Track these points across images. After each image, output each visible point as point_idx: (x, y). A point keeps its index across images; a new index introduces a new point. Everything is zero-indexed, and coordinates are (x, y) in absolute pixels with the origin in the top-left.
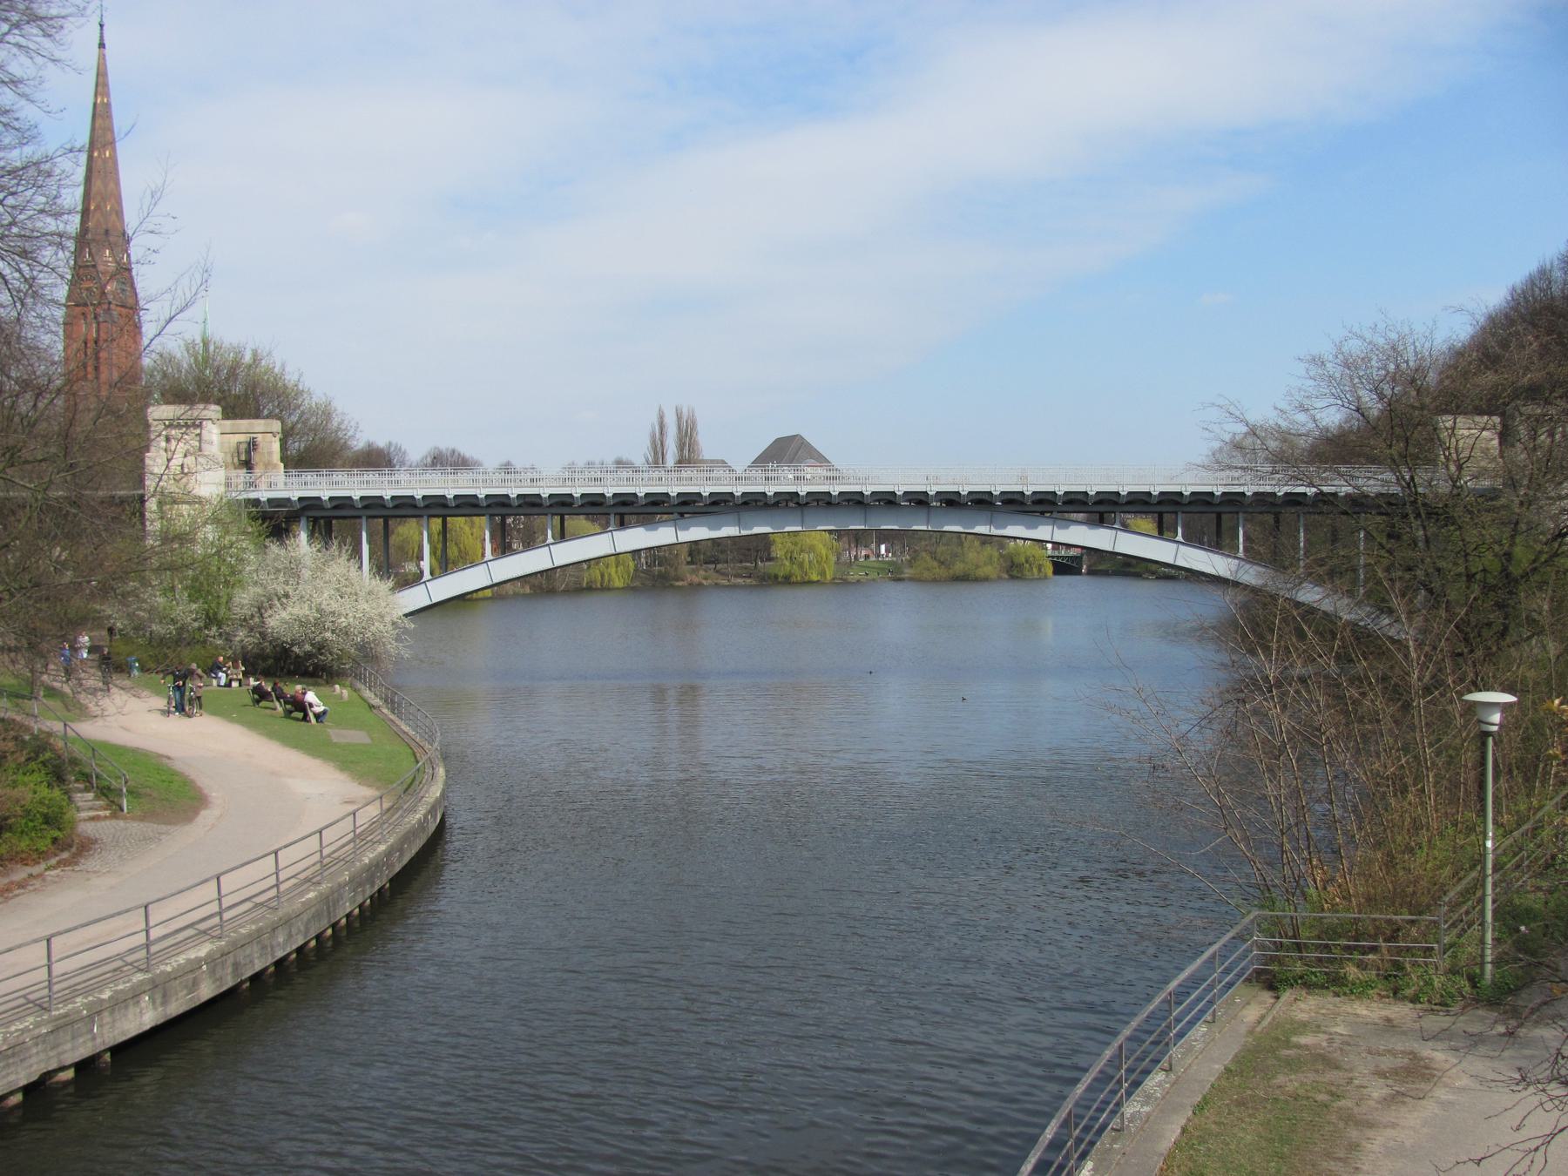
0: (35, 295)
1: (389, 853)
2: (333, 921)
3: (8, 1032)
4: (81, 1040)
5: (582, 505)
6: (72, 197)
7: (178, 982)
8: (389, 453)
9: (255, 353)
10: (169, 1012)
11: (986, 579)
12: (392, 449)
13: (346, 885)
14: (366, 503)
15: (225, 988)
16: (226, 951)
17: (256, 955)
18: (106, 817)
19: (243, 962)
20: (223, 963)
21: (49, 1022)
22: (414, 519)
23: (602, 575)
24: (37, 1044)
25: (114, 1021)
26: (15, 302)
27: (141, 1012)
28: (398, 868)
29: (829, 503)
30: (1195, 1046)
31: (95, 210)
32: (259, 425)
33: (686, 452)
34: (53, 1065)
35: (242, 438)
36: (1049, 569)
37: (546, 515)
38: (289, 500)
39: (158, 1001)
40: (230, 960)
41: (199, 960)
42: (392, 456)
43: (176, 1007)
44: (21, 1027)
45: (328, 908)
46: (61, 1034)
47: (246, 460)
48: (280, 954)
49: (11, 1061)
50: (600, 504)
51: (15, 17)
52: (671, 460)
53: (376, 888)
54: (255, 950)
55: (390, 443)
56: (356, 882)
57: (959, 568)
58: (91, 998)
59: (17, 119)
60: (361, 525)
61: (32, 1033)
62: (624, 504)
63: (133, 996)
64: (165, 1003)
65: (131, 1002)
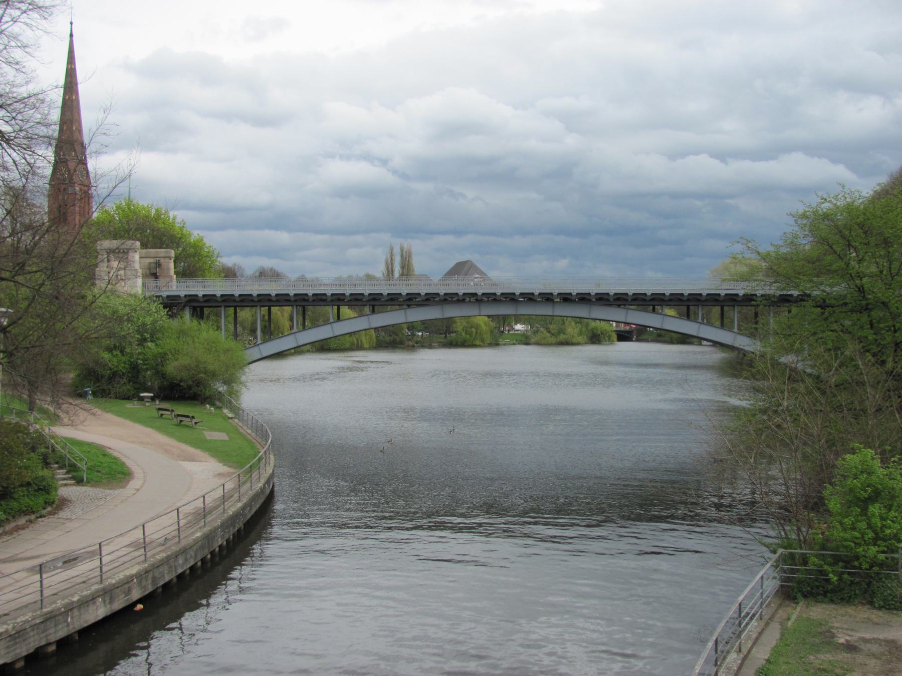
0: (34, 174)
1: (243, 508)
2: (211, 550)
3: (15, 623)
4: (60, 627)
5: (350, 300)
6: (55, 115)
7: (119, 589)
8: (234, 270)
9: (157, 211)
10: (113, 608)
11: (578, 344)
12: (236, 267)
13: (218, 528)
14: (206, 299)
15: (147, 593)
16: (148, 570)
17: (166, 572)
18: (71, 485)
19: (158, 576)
20: (146, 578)
21: (41, 616)
22: (248, 308)
23: (357, 340)
24: (33, 630)
25: (80, 615)
26: (21, 177)
27: (97, 609)
28: (249, 516)
29: (495, 300)
30: (752, 635)
31: (67, 129)
32: (162, 252)
33: (405, 270)
34: (43, 643)
35: (152, 260)
36: (615, 337)
37: (256, 306)
38: (179, 296)
39: (107, 601)
40: (150, 575)
41: (132, 576)
42: (236, 271)
43: (118, 605)
44: (24, 619)
45: (208, 542)
46: (48, 623)
47: (153, 273)
48: (180, 571)
49: (17, 640)
50: (360, 300)
51: (24, 7)
52: (397, 274)
53: (236, 529)
54: (165, 568)
55: (235, 265)
56: (224, 526)
57: (562, 337)
58: (66, 601)
59: (24, 67)
60: (221, 310)
61: (30, 623)
62: (374, 299)
63: (93, 599)
64: (111, 602)
65: (91, 602)
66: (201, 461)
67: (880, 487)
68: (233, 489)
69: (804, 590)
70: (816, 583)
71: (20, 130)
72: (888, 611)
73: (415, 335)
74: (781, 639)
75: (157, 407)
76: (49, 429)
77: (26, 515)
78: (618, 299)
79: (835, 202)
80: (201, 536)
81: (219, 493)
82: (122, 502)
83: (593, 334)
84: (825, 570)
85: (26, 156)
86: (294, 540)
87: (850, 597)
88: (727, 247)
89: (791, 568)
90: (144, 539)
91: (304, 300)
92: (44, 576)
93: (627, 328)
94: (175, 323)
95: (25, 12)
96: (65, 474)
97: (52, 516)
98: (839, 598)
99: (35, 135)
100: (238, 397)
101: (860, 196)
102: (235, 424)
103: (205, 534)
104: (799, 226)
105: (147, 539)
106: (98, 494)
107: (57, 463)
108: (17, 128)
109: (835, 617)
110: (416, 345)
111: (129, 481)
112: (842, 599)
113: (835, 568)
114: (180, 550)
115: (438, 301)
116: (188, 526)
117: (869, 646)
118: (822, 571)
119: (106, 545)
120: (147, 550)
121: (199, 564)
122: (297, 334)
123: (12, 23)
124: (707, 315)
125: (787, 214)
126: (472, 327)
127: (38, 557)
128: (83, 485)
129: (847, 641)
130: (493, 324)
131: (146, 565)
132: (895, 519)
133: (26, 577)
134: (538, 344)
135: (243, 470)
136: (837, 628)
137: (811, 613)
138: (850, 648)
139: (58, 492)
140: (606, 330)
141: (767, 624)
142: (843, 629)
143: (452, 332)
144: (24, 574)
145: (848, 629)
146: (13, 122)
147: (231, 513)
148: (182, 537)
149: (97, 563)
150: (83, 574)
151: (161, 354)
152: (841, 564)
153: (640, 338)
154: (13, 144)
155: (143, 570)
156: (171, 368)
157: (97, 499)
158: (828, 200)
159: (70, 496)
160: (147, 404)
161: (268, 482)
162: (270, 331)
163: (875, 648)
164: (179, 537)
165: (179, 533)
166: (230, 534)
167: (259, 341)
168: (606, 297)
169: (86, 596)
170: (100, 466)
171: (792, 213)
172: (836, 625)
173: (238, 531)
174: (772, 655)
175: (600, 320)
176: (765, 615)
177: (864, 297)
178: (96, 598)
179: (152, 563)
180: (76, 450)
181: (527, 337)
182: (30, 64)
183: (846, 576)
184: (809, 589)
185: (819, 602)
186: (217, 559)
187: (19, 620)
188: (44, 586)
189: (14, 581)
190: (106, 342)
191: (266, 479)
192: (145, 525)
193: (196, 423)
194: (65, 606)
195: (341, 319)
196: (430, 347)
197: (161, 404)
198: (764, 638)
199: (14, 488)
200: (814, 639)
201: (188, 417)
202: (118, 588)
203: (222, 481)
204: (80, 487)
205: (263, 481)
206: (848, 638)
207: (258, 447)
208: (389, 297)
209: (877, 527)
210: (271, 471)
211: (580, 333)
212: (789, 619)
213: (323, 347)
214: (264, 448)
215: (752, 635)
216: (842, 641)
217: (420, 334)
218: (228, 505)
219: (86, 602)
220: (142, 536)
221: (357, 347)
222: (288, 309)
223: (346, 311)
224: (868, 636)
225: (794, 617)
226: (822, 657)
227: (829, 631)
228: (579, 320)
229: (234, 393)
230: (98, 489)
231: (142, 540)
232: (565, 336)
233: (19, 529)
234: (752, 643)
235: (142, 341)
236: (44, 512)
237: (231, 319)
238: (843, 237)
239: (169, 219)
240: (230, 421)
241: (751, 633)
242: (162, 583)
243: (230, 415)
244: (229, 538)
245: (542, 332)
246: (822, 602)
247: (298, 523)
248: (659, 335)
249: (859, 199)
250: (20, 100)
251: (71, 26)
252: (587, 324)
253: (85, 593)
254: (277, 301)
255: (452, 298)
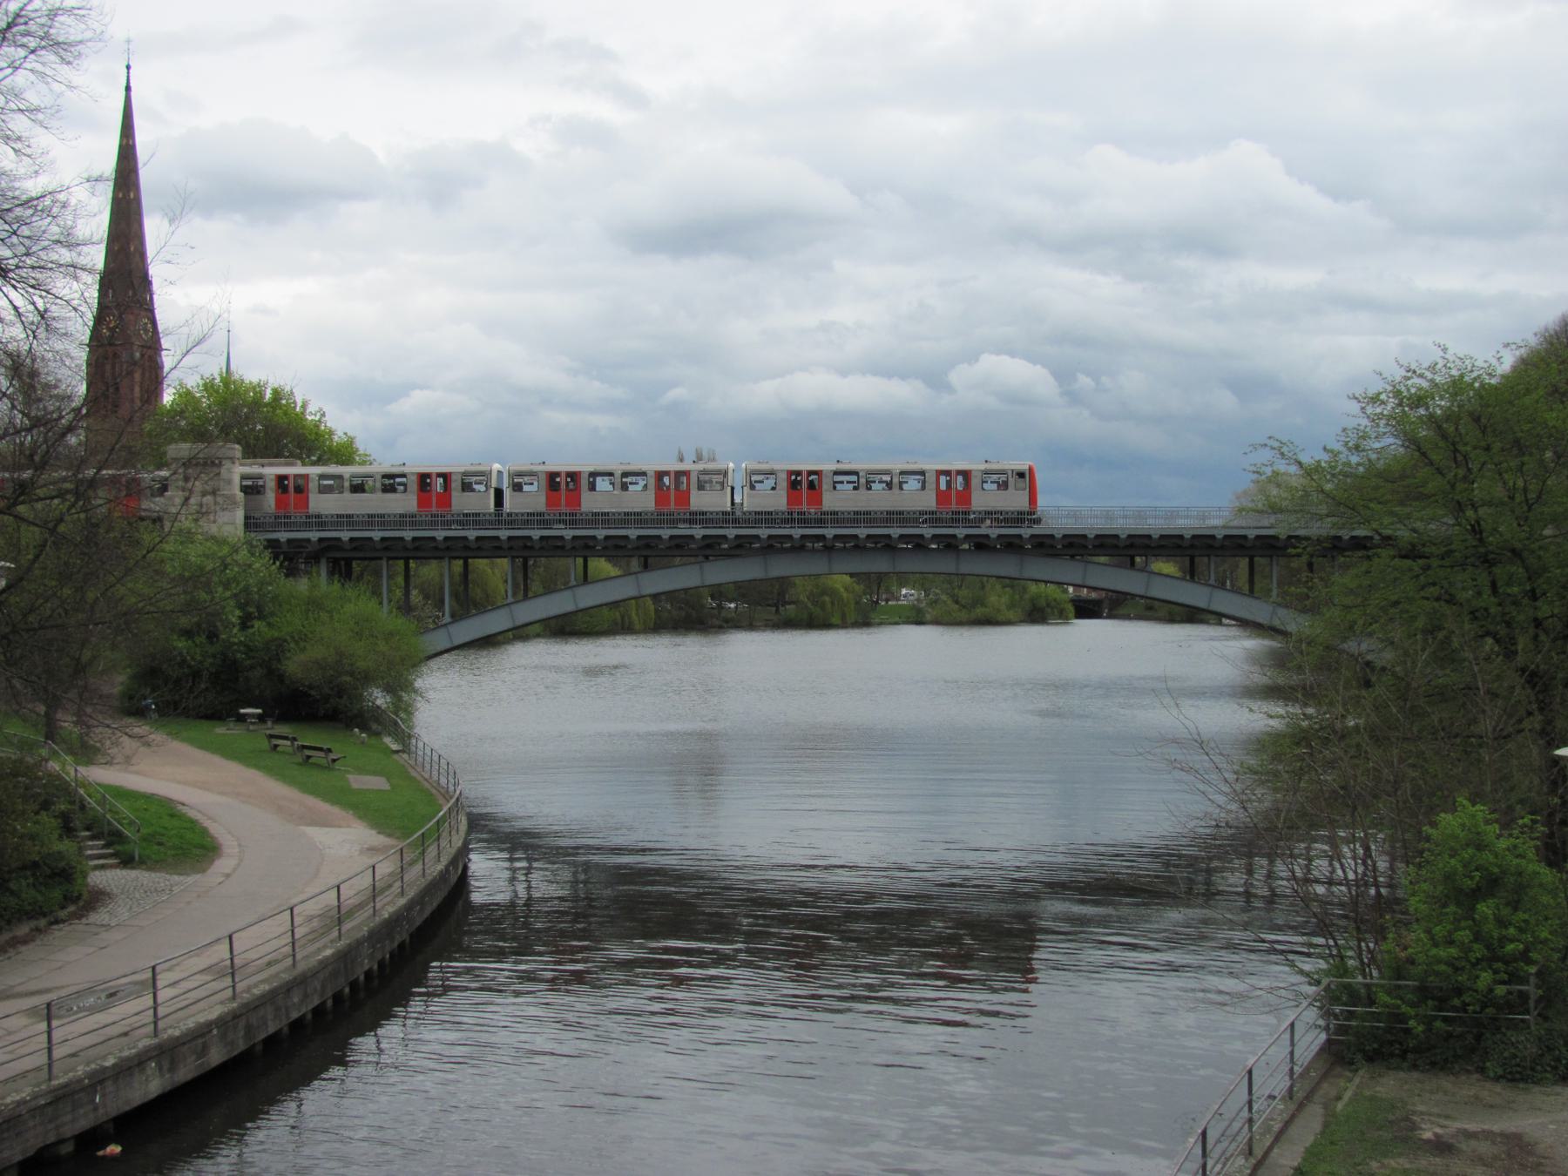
1: (409, 907)
4: (82, 1111)
7: (186, 1047)
10: (176, 1079)
14: (354, 545)
15: (235, 1053)
21: (51, 1092)
23: (623, 617)
26: (28, 336)
28: (418, 922)
29: (856, 547)
30: (1273, 1126)
34: (52, 1139)
36: (1070, 608)
37: (441, 558)
40: (242, 1023)
41: (209, 1025)
43: (185, 1073)
44: (18, 1098)
48: (295, 1015)
51: (33, 43)
53: (396, 944)
57: (979, 611)
58: (93, 1066)
64: (172, 1069)
66: (340, 827)
67: (1496, 870)
68: (390, 875)
69: (1367, 1048)
70: (1389, 1037)
71: (27, 254)
72: (1510, 1084)
73: (723, 608)
74: (1323, 1133)
75: (268, 732)
76: (76, 770)
77: (30, 918)
78: (1071, 545)
79: (1429, 375)
80: (333, 955)
81: (366, 881)
82: (199, 896)
83: (1034, 605)
84: (1404, 1014)
85: (36, 299)
86: (764, 1016)
87: (1446, 1061)
88: (1245, 453)
89: (1347, 1011)
90: (232, 959)
91: (526, 547)
92: (55, 1023)
93: (1094, 595)
94: (302, 585)
95: (33, 52)
96: (102, 848)
97: (77, 921)
98: (1428, 1061)
99: (51, 262)
100: (410, 714)
101: (1473, 366)
102: (402, 762)
103: (339, 951)
104: (1368, 417)
105: (236, 961)
106: (159, 883)
107: (88, 829)
108: (22, 250)
109: (1419, 1095)
110: (725, 625)
111: (213, 861)
112: (1433, 1064)
113: (1421, 1011)
114: (295, 978)
115: (757, 549)
116: (310, 937)
117: (1473, 1143)
118: (1399, 1015)
119: (168, 970)
120: (237, 980)
121: (330, 1003)
122: (513, 607)
123: (9, 71)
124: (1232, 573)
125: (1348, 397)
126: (824, 593)
127: (48, 991)
128: (133, 868)
129: (1436, 1135)
130: (859, 588)
131: (235, 1005)
132: (1523, 924)
133: (25, 1026)
134: (937, 622)
135: (408, 841)
136: (1422, 1113)
137: (1378, 1089)
138: (1442, 1147)
139: (89, 880)
140: (1055, 600)
141: (1301, 1106)
142: (1430, 1115)
143: (790, 603)
144: (24, 1021)
145: (1439, 1116)
146: (15, 239)
147: (387, 916)
148: (298, 957)
149: (148, 1000)
150: (123, 1019)
151: (277, 639)
152: (1430, 1003)
153: (1115, 612)
154: (13, 279)
155: (228, 1013)
156: (294, 665)
157: (156, 890)
158: (1418, 372)
159: (109, 885)
160: (251, 727)
161: (454, 862)
162: (468, 601)
163: (1484, 1148)
164: (294, 956)
165: (294, 950)
166: (386, 949)
167: (447, 619)
168: (1048, 542)
169: (128, 1059)
170: (163, 835)
171: (1357, 395)
172: (1421, 1108)
173: (399, 946)
174: (1304, 1159)
175: (1046, 582)
176: (1298, 1092)
177: (1481, 540)
178: (147, 1061)
179: (245, 1001)
180: (123, 807)
181: (919, 611)
182: (41, 139)
183: (1438, 1024)
184: (1375, 1046)
185: (1394, 1069)
186: (362, 995)
187: (8, 1100)
188: (54, 1042)
189: (5, 1032)
190: (184, 621)
191: (451, 856)
192: (234, 936)
193: (334, 761)
194: (91, 1075)
195: (589, 580)
196: (751, 626)
197: (276, 727)
198: (1293, 1131)
199: (9, 872)
200: (1381, 1133)
201: (320, 749)
202: (184, 1044)
203: (371, 862)
204: (129, 871)
205: (444, 861)
206: (1439, 1130)
207: (440, 802)
208: (673, 543)
209: (1492, 937)
210: (460, 844)
211: (1011, 606)
212: (1339, 1098)
213: (564, 628)
214: (448, 801)
215: (1273, 1126)
216: (1427, 1135)
217: (732, 605)
218: (382, 903)
219: (127, 1069)
220: (228, 955)
221: (623, 628)
222: (504, 563)
223: (600, 566)
224: (1472, 1127)
225: (1348, 1095)
226: (1393, 1163)
227: (1407, 1119)
228: (1010, 582)
229: (404, 709)
230: (158, 874)
231: (229, 962)
232: (983, 609)
233: (19, 942)
234: (1271, 1140)
235: (245, 623)
236: (62, 914)
237: (400, 580)
238: (1444, 436)
239: (295, 407)
240: (395, 757)
241: (1272, 1123)
242: (263, 1036)
243: (395, 747)
244: (384, 958)
245: (945, 602)
246: (1398, 1068)
247: (712, 978)
248: (1150, 608)
249: (1472, 371)
250: (26, 202)
251: (128, 73)
252: (1025, 589)
253: (126, 1053)
254: (479, 548)
255: (782, 543)
